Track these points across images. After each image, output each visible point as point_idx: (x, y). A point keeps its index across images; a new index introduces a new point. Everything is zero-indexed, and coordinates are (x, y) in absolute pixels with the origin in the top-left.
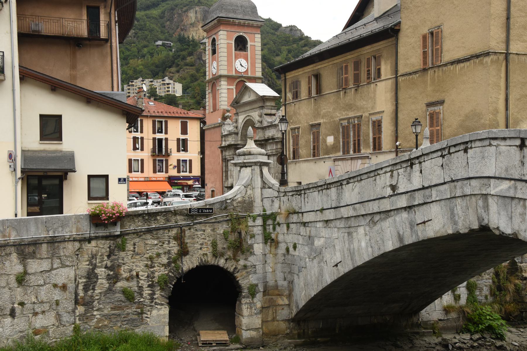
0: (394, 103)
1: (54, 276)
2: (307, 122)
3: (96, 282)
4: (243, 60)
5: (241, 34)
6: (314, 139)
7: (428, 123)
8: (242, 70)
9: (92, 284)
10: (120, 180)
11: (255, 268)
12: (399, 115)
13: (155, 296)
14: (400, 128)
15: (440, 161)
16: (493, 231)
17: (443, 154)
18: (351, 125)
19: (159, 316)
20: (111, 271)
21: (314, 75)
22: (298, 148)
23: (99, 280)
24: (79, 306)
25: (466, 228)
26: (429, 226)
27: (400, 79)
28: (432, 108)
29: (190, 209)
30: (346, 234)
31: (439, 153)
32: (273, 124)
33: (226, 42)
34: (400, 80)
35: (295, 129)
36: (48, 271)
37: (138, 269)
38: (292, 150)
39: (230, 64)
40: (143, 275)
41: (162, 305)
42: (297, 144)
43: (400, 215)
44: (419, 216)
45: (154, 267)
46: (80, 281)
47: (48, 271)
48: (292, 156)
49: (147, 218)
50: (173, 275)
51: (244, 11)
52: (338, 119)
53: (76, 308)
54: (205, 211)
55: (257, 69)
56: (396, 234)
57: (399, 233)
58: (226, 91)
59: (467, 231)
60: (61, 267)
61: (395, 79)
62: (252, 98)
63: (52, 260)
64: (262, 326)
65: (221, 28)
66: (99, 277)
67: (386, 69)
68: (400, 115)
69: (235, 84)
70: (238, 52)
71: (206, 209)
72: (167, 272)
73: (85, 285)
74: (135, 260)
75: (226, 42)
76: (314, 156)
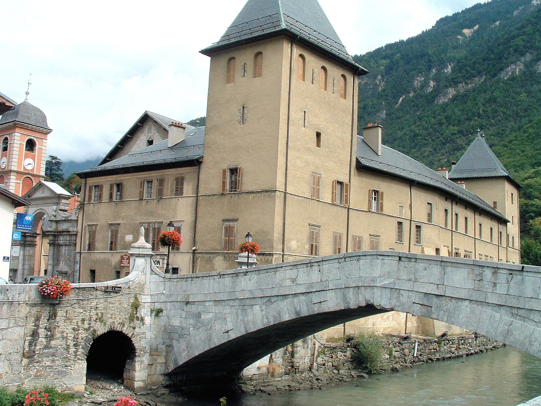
0: (194, 216)
1: (9, 334)
2: (105, 221)
3: (37, 340)
4: (31, 160)
5: (32, 137)
6: (112, 236)
7: (223, 234)
8: (29, 168)
9: (35, 341)
10: (4, 258)
11: (145, 334)
12: (197, 225)
13: (78, 353)
14: (198, 235)
15: (337, 265)
16: (376, 307)
17: (340, 262)
18: (151, 228)
19: (450, 321)
20: (50, 331)
21: (116, 184)
22: (95, 242)
23: (40, 339)
24: (24, 358)
25: (356, 305)
26: (324, 304)
27: (200, 198)
28: (228, 223)
29: (107, 286)
30: (239, 311)
31: (337, 261)
32: (69, 218)
33: (20, 142)
34: (200, 198)
35: (92, 225)
36: (6, 329)
37: (67, 331)
38: (87, 243)
39: (20, 162)
40: (71, 336)
41: (82, 360)
42: (94, 238)
43: (298, 297)
44: (315, 298)
45: (79, 330)
46: (27, 338)
47: (6, 329)
48: (87, 247)
49: (77, 291)
50: (91, 337)
51: (36, 119)
52: (139, 222)
53: (22, 360)
54: (116, 289)
55: (41, 169)
56: (294, 310)
57: (295, 309)
58: (14, 184)
59: (356, 307)
60: (15, 327)
61: (196, 197)
62: (47, 194)
63: (9, 321)
64: (147, 378)
65: (17, 130)
66: (40, 336)
67: (188, 188)
68: (198, 225)
69: (22, 179)
70: (28, 152)
71: (117, 287)
72: (87, 335)
73: (30, 342)
74: (66, 324)
75: (20, 142)
76: (111, 249)
